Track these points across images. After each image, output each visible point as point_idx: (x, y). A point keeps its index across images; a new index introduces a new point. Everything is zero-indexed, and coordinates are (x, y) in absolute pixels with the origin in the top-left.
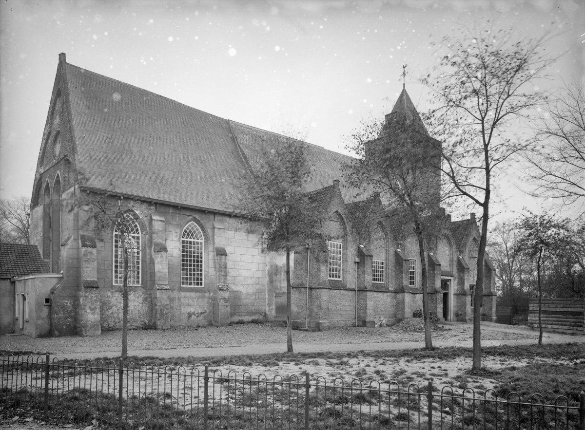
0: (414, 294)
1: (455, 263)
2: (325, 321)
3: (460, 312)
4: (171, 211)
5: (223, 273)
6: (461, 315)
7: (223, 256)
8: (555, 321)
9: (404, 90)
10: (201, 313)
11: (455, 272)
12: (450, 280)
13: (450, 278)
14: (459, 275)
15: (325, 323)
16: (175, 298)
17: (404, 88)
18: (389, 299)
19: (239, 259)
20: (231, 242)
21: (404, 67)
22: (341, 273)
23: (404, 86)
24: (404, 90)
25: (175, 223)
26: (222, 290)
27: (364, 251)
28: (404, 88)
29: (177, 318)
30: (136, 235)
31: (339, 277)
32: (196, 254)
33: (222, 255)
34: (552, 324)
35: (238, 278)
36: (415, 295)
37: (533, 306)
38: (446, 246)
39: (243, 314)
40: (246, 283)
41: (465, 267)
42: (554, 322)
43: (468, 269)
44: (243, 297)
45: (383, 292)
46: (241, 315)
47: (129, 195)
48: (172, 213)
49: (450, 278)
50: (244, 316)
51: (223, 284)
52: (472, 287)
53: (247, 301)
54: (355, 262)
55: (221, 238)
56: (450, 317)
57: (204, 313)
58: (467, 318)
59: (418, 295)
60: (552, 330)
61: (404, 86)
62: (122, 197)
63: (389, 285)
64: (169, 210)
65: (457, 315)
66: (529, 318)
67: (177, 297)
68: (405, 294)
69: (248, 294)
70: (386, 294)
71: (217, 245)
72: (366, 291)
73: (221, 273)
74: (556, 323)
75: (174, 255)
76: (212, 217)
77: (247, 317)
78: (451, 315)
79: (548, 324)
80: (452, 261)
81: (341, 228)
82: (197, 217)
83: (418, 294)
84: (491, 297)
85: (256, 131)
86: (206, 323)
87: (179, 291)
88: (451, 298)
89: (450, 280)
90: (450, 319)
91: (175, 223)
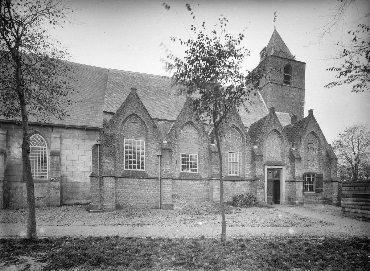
0: (234, 181)
1: (287, 155)
2: (110, 204)
3: (292, 197)
4: (13, 127)
5: (55, 169)
6: (293, 199)
7: (55, 157)
8: (363, 205)
9: (275, 32)
10: (41, 198)
11: (287, 161)
12: (282, 169)
13: (280, 167)
14: (291, 165)
15: (109, 206)
16: (18, 187)
17: (275, 29)
18: (201, 186)
19: (77, 159)
20: (69, 147)
21: (275, 14)
22: (144, 165)
23: (275, 28)
24: (275, 32)
25: (18, 135)
26: (53, 181)
27: (256, 151)
28: (275, 29)
29: (19, 201)
30: (43, 147)
31: (142, 168)
32: (192, 165)
33: (54, 156)
34: (362, 209)
35: (76, 172)
36: (235, 182)
37: (345, 190)
38: (277, 140)
39: (80, 198)
40: (84, 176)
41: (296, 156)
42: (363, 207)
43: (300, 159)
44: (80, 186)
45: (194, 180)
46: (79, 199)
47: (11, 120)
48: (14, 128)
49: (280, 167)
50: (82, 200)
51: (55, 177)
52: (313, 175)
53: (85, 189)
54: (158, 156)
55: (57, 144)
56: (282, 201)
57: (44, 197)
58: (297, 202)
59: (239, 182)
60: (361, 215)
61: (275, 28)
62: (86, 129)
63: (202, 174)
64: (12, 127)
65: (290, 199)
66: (342, 202)
67: (19, 186)
68: (214, 181)
69: (85, 184)
70: (198, 182)
71: (53, 149)
72: (296, 181)
73: (53, 169)
74: (365, 207)
75: (17, 157)
76: (50, 129)
77: (85, 200)
78: (283, 199)
79: (357, 209)
80: (283, 153)
81: (143, 128)
82: (37, 130)
83: (239, 181)
84: (331, 183)
85: (132, 74)
86: (46, 205)
87: (22, 183)
88: (282, 185)
89: (282, 169)
90: (282, 203)
91: (18, 135)
